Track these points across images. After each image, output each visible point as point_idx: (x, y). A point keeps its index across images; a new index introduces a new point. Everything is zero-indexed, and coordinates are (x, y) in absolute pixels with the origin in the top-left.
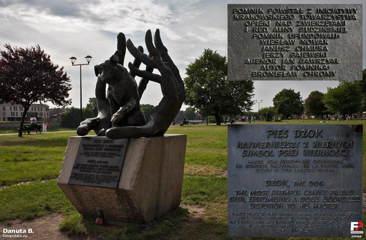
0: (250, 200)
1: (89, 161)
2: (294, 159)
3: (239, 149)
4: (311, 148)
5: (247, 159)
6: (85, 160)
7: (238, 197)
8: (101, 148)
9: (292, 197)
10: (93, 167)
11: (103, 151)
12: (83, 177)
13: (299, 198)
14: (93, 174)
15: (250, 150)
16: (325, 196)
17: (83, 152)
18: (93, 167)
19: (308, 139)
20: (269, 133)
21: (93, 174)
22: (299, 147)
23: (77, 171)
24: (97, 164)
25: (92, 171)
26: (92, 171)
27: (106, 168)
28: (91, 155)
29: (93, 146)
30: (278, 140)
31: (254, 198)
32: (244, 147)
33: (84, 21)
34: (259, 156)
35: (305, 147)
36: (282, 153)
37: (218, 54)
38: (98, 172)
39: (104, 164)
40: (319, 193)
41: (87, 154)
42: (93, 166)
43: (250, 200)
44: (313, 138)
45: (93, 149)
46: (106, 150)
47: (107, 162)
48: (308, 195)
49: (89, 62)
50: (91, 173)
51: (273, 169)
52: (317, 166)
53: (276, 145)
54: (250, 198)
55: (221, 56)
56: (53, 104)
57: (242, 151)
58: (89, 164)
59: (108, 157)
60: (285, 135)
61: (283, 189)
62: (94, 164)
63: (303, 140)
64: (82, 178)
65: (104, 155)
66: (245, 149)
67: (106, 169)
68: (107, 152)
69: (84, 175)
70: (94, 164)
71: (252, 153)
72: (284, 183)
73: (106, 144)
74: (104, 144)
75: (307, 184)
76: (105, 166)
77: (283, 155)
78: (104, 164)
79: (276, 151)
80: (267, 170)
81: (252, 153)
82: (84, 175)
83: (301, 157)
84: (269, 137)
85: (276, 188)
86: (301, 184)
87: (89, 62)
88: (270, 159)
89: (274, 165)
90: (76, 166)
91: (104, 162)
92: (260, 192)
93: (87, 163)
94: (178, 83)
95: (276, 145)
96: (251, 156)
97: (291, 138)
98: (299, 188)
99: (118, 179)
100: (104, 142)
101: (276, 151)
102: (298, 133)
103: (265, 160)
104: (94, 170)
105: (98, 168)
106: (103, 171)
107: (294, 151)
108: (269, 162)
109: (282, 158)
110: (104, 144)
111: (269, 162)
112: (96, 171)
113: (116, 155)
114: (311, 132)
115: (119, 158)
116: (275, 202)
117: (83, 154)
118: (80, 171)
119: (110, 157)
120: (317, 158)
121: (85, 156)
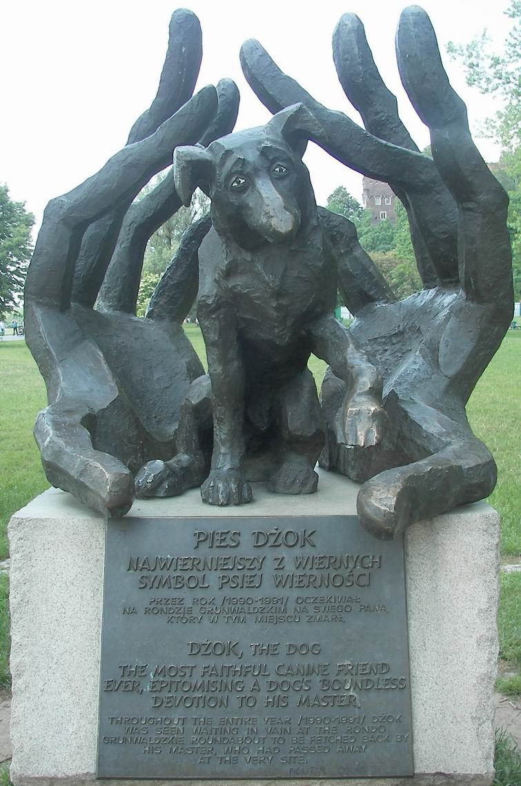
1: (196, 649)
2: (257, 594)
4: (290, 568)
9: (249, 682)
11: (268, 589)
13: (263, 682)
15: (154, 574)
16: (326, 678)
17: (141, 599)
19: (283, 552)
23: (140, 706)
30: (216, 553)
39: (297, 661)
40: (310, 671)
41: (177, 613)
43: (153, 687)
45: (201, 585)
47: (315, 650)
51: (206, 617)
52: (304, 610)
57: (138, 575)
58: (202, 662)
63: (268, 552)
65: (274, 613)
66: (145, 573)
72: (230, 649)
78: (297, 661)
79: (213, 578)
80: (192, 620)
84: (197, 547)
85: (211, 661)
86: (272, 650)
88: (199, 594)
91: (293, 649)
98: (264, 660)
102: (261, 537)
103: (187, 595)
109: (227, 592)
111: (195, 601)
112: (263, 696)
114: (289, 534)
120: (306, 593)
121: (161, 620)
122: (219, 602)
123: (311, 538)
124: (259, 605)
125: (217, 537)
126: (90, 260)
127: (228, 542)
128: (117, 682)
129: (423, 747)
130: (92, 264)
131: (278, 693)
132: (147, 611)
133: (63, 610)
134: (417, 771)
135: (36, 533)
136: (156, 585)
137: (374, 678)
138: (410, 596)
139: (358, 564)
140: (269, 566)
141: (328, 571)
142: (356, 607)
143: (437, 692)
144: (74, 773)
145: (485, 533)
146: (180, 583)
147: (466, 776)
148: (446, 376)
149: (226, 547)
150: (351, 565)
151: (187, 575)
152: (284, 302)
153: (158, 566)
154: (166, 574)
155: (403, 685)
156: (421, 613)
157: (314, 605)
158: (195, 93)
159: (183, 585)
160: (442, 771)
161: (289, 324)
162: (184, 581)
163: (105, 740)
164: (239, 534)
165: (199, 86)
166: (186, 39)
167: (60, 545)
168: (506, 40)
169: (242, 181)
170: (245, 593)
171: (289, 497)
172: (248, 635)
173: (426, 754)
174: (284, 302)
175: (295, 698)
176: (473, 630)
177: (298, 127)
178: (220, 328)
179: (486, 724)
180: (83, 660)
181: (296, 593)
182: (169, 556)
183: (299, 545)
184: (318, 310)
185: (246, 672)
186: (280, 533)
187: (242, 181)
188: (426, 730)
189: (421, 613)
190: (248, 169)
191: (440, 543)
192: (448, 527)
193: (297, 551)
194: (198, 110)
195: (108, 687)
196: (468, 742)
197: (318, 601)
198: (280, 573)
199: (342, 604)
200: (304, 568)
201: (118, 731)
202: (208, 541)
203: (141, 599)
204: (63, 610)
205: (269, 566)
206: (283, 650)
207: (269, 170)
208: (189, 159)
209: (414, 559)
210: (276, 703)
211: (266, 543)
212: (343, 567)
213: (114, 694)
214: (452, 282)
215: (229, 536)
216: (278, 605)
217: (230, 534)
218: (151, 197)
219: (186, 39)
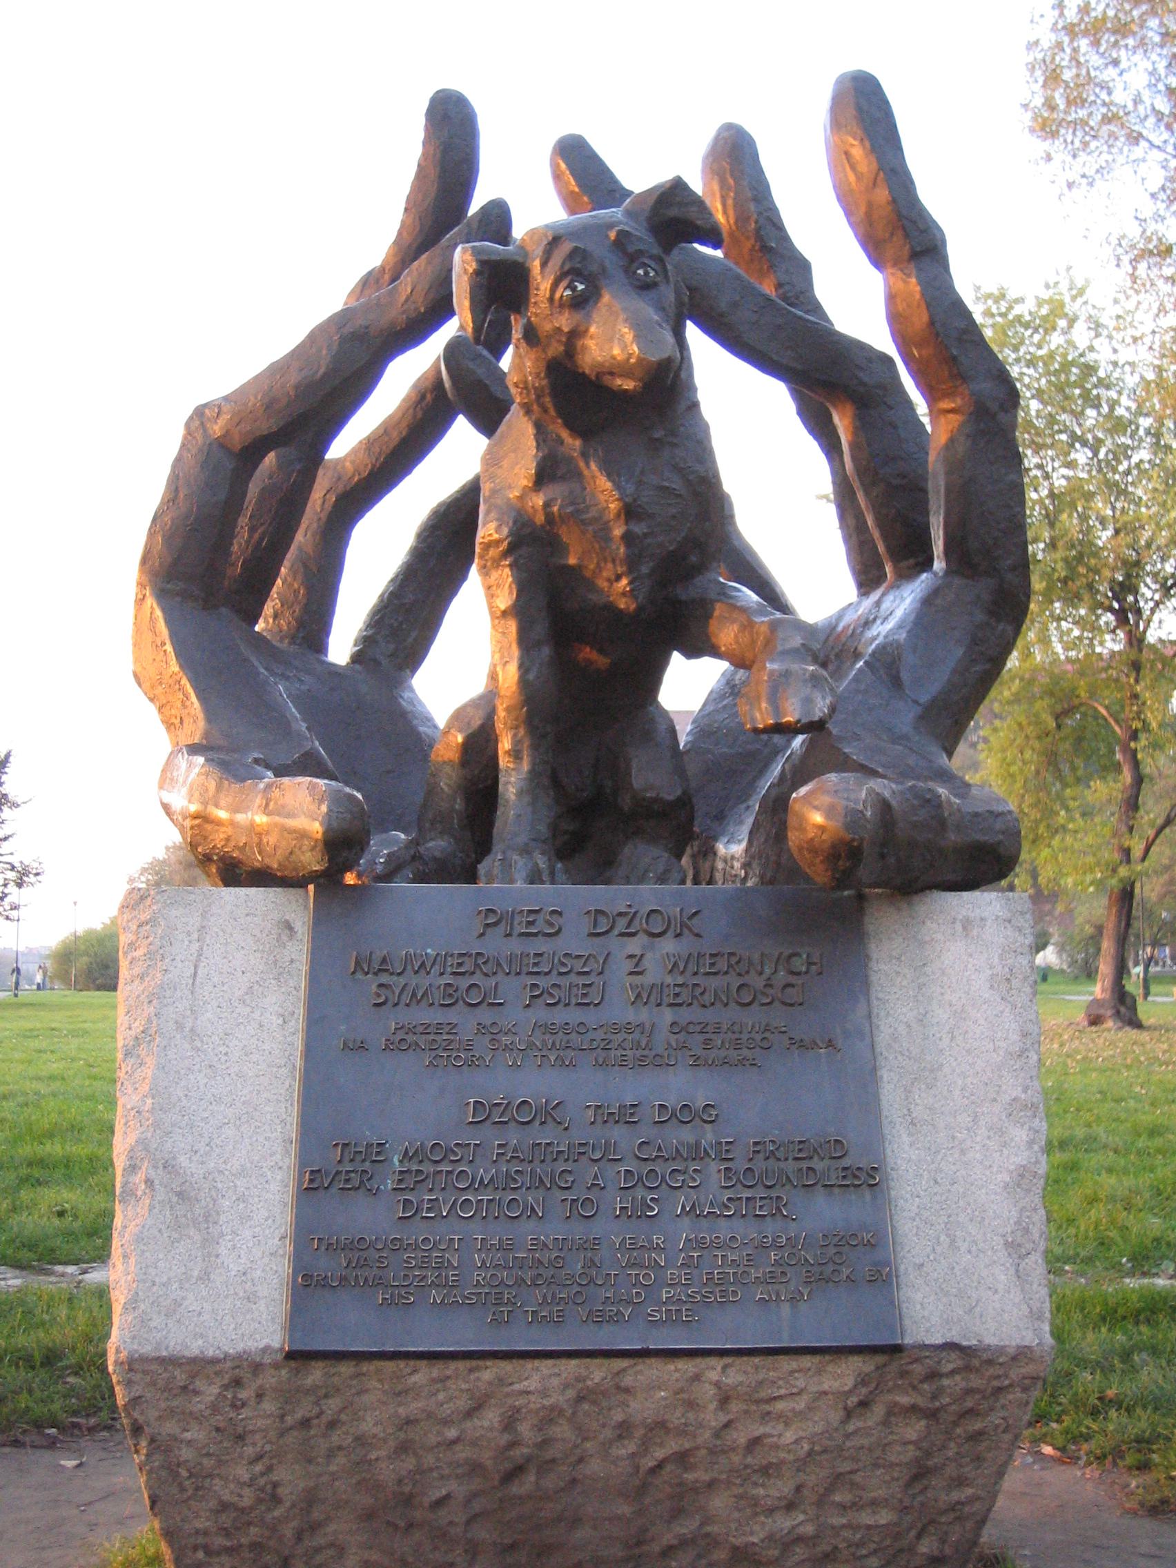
0: (400, 1181)
2: (590, 1017)
3: (359, 976)
5: (392, 1020)
6: (416, 1106)
7: (348, 1172)
11: (620, 1010)
15: (402, 981)
20: (486, 917)
22: (607, 972)
30: (516, 946)
31: (419, 1172)
32: (380, 970)
33: (917, 564)
34: (442, 1005)
35: (631, 973)
41: (441, 1048)
43: (400, 1181)
44: (478, 1010)
48: (653, 1160)
53: (517, 966)
54: (401, 1172)
56: (11, 759)
58: (492, 1138)
60: (551, 925)
61: (545, 1135)
66: (384, 978)
71: (414, 995)
72: (549, 1114)
77: (540, 1001)
81: (414, 995)
84: (482, 935)
85: (513, 1137)
86: (627, 1116)
88: (485, 1016)
89: (505, 1039)
95: (517, 966)
96: (407, 1005)
97: (574, 941)
98: (617, 1133)
102: (602, 920)
103: (466, 1022)
107: (590, 985)
109: (540, 1014)
114: (654, 916)
116: (508, 1191)
120: (685, 1015)
123: (695, 921)
124: (600, 1034)
125: (517, 919)
126: (257, 536)
127: (540, 926)
128: (332, 1170)
129: (919, 1296)
130: (261, 539)
131: (640, 1193)
133: (223, 1049)
134: (908, 1340)
135: (174, 913)
136: (406, 998)
137: (817, 1164)
138: (878, 1027)
139: (781, 967)
141: (727, 978)
143: (937, 1198)
144: (240, 1347)
145: (1007, 924)
146: (451, 998)
147: (1001, 1350)
148: (915, 702)
149: (535, 935)
150: (768, 971)
151: (464, 983)
152: (639, 528)
153: (409, 967)
154: (423, 981)
155: (866, 1179)
156: (900, 1058)
157: (701, 1038)
158: (471, 212)
159: (456, 1001)
160: (956, 1340)
161: (645, 570)
162: (459, 993)
163: (307, 1285)
164: (560, 914)
165: (474, 208)
166: (452, 134)
167: (221, 934)
168: (1042, 16)
169: (580, 287)
170: (573, 1016)
172: (581, 1089)
173: (923, 1308)
174: (639, 528)
177: (673, 212)
179: (1033, 1257)
180: (261, 1139)
181: (668, 1015)
182: (429, 951)
183: (670, 934)
184: (694, 559)
185: (579, 1152)
186: (635, 913)
187: (580, 287)
188: (922, 1265)
189: (900, 1058)
190: (594, 268)
191: (927, 938)
192: (941, 912)
193: (668, 945)
195: (315, 1184)
196: (1001, 1287)
197: (708, 1029)
198: (637, 980)
199: (753, 1035)
200: (682, 973)
201: (325, 1265)
202: (504, 922)
204: (223, 1049)
207: (629, 272)
208: (486, 258)
209: (882, 966)
210: (638, 1213)
211: (612, 928)
212: (752, 972)
213: (322, 1193)
215: (540, 919)
216: (636, 1035)
217: (542, 914)
218: (370, 443)
219: (452, 134)
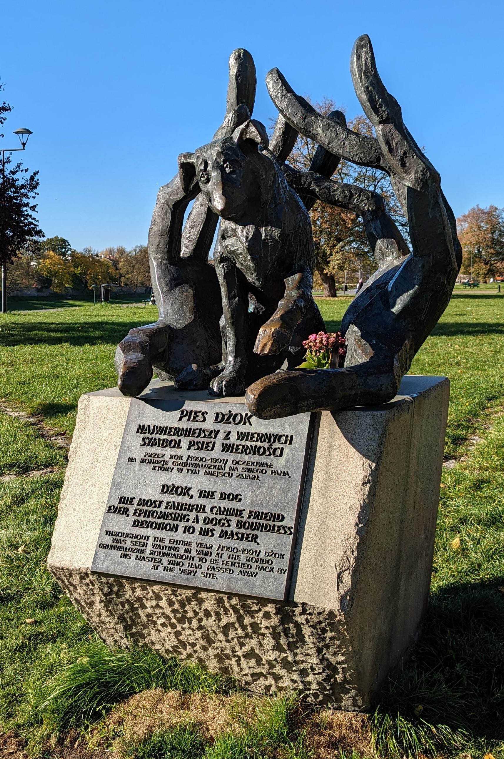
1: (165, 489)
4: (233, 438)
6: (148, 485)
8: (206, 440)
9: (192, 515)
10: (185, 513)
11: (217, 453)
12: (149, 548)
13: (201, 516)
14: (187, 537)
18: (185, 513)
19: (230, 427)
21: (187, 537)
23: (123, 524)
24: (197, 501)
25: (181, 529)
26: (181, 529)
27: (234, 520)
28: (170, 465)
29: (178, 431)
36: (191, 445)
37: (107, 250)
38: (205, 533)
39: (225, 504)
41: (159, 464)
42: (181, 507)
45: (178, 445)
46: (227, 448)
47: (237, 498)
49: (24, 144)
50: (180, 535)
53: (188, 432)
55: (135, 250)
58: (167, 498)
59: (240, 476)
62: (185, 500)
64: (143, 552)
65: (216, 469)
67: (233, 523)
68: (230, 457)
69: (151, 541)
70: (185, 500)
72: (185, 491)
73: (223, 428)
74: (217, 427)
75: (217, 496)
76: (229, 512)
78: (225, 504)
79: (185, 442)
80: (167, 469)
82: (151, 541)
83: (217, 453)
86: (209, 495)
87: (24, 144)
90: (120, 507)
91: (223, 496)
92: (152, 503)
93: (157, 497)
94: (414, 218)
98: (202, 501)
99: (285, 564)
100: (217, 418)
101: (185, 442)
103: (168, 452)
104: (190, 524)
105: (205, 519)
106: (225, 529)
108: (171, 457)
110: (217, 427)
111: (171, 457)
112: (198, 527)
113: (269, 471)
115: (282, 482)
117: (143, 461)
118: (136, 524)
119: (246, 477)
121: (148, 468)
122: (185, 459)
132: (143, 461)
140: (221, 436)
142: (269, 471)
146: (167, 443)
171: (195, 392)
172: (198, 482)
175: (218, 529)
176: (348, 498)
178: (225, 274)
185: (191, 508)
194: (232, 123)
203: (139, 452)
205: (221, 436)
206: (217, 496)
214: (231, 669)
